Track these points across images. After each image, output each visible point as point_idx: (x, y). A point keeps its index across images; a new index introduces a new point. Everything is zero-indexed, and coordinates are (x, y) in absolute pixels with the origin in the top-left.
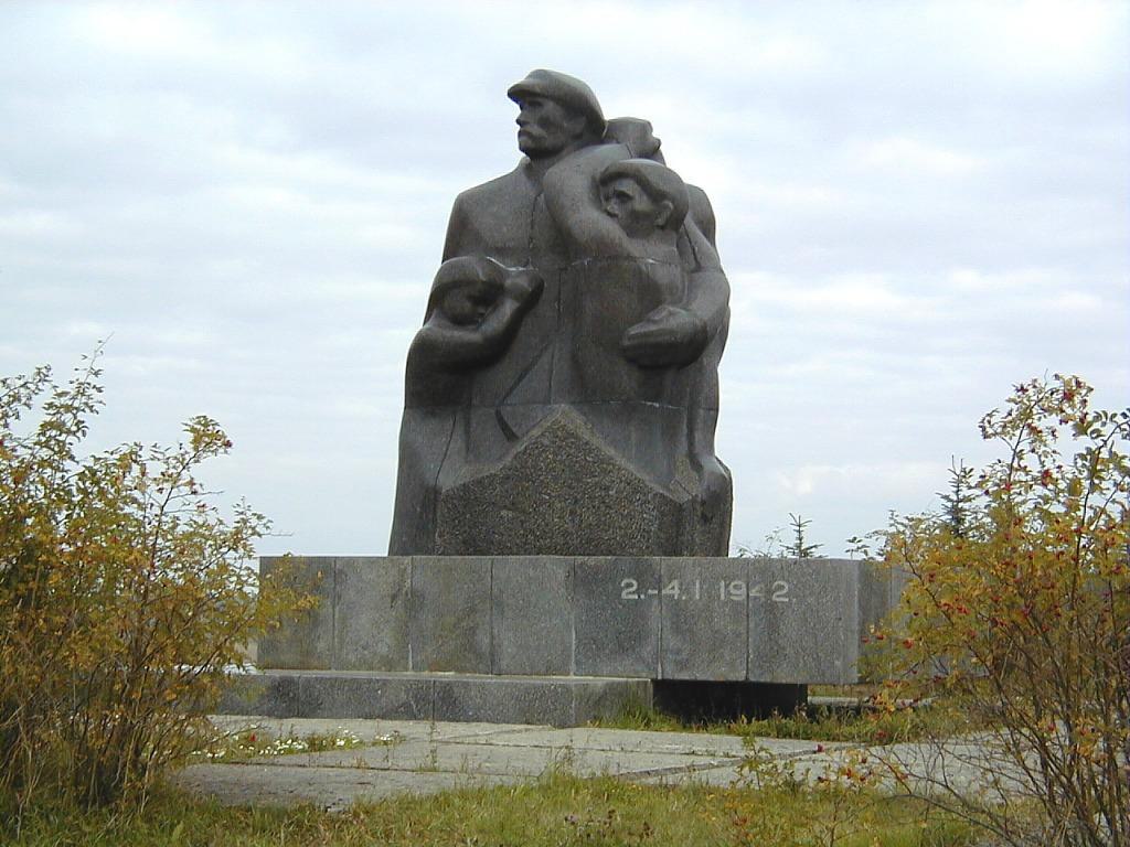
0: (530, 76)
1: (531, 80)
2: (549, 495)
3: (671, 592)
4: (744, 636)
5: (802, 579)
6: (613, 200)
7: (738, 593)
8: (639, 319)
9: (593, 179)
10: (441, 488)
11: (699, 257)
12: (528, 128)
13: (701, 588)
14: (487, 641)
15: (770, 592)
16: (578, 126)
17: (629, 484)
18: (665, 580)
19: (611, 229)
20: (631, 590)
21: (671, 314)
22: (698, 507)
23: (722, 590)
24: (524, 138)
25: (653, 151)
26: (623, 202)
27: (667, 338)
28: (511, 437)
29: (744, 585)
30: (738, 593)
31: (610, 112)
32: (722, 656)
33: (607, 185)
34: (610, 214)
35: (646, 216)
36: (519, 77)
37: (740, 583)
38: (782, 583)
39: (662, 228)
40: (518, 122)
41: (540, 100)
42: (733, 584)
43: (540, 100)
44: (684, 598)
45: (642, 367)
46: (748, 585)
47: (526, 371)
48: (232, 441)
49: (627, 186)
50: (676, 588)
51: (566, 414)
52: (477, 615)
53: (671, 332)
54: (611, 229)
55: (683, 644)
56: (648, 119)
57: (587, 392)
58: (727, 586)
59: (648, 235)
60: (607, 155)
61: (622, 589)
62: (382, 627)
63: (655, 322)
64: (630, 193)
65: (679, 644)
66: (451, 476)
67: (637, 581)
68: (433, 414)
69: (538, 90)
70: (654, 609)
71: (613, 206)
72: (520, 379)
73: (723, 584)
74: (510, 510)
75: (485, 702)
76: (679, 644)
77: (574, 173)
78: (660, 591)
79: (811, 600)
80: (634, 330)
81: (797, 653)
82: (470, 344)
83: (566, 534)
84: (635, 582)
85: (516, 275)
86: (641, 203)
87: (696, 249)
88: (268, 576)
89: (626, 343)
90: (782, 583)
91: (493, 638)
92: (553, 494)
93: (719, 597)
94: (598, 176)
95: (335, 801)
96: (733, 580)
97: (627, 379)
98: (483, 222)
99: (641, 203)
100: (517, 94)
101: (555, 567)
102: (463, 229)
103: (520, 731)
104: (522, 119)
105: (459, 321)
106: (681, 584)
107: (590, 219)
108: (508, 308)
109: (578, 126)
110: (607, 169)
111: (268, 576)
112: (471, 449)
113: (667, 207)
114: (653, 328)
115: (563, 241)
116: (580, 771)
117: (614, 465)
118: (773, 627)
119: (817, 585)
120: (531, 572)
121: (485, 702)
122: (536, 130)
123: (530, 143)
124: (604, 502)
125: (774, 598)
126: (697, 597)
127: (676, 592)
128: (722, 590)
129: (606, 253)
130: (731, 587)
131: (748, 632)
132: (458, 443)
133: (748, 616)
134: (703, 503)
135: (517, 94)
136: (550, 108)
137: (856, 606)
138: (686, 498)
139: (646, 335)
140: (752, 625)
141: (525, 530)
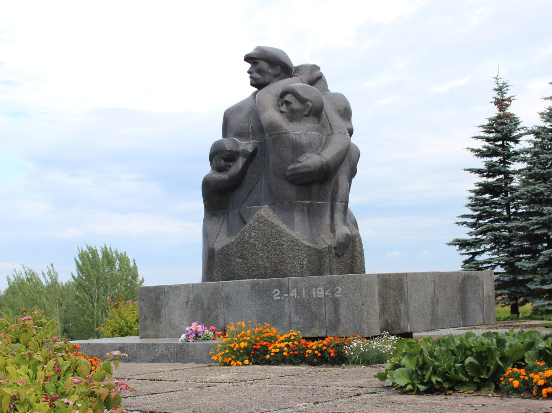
0: (254, 50)
1: (255, 51)
2: (256, 250)
3: (293, 295)
4: (324, 315)
5: (347, 285)
6: (284, 105)
7: (321, 293)
8: (293, 162)
9: (277, 96)
10: (215, 250)
11: (333, 127)
12: (253, 75)
13: (305, 292)
14: (223, 322)
15: (333, 292)
16: (278, 70)
17: (292, 242)
18: (290, 288)
20: (278, 294)
21: (308, 158)
22: (333, 250)
23: (314, 292)
26: (288, 105)
27: (306, 169)
28: (245, 223)
29: (323, 290)
30: (321, 293)
31: (296, 61)
32: (315, 325)
34: (282, 112)
35: (298, 111)
36: (250, 50)
37: (321, 288)
38: (338, 288)
39: (307, 116)
40: (249, 72)
41: (257, 61)
42: (318, 289)
43: (257, 61)
44: (299, 297)
45: (297, 185)
46: (324, 290)
47: (251, 191)
49: (288, 98)
50: (295, 292)
52: (219, 310)
53: (308, 167)
55: (300, 320)
56: (320, 67)
58: (316, 290)
59: (300, 120)
61: (274, 294)
62: (183, 317)
63: (300, 162)
64: (290, 101)
65: (298, 320)
67: (279, 290)
68: (215, 215)
69: (255, 56)
70: (287, 304)
71: (284, 108)
72: (248, 195)
73: (314, 290)
74: (241, 258)
75: (195, 354)
76: (298, 320)
78: (289, 295)
79: (351, 295)
80: (290, 167)
81: (346, 322)
82: (223, 181)
83: (265, 268)
84: (279, 291)
86: (296, 105)
87: (332, 124)
89: (288, 174)
90: (338, 288)
91: (225, 320)
92: (258, 249)
93: (313, 296)
94: (279, 94)
95: (317, 371)
96: (318, 287)
97: (290, 191)
98: (234, 122)
99: (296, 105)
100: (248, 59)
101: (246, 283)
104: (250, 71)
106: (297, 291)
108: (241, 162)
109: (278, 70)
110: (284, 88)
112: (230, 232)
113: (308, 105)
114: (299, 165)
116: (471, 342)
117: (285, 233)
118: (336, 310)
119: (353, 288)
120: (238, 288)
121: (195, 354)
122: (257, 75)
123: (254, 82)
124: (281, 252)
125: (336, 296)
126: (304, 297)
127: (295, 294)
128: (314, 292)
130: (317, 291)
131: (325, 312)
132: (224, 228)
133: (325, 305)
134: (335, 248)
135: (248, 59)
137: (377, 297)
138: (325, 246)
139: (295, 169)
140: (327, 309)
141: (247, 267)
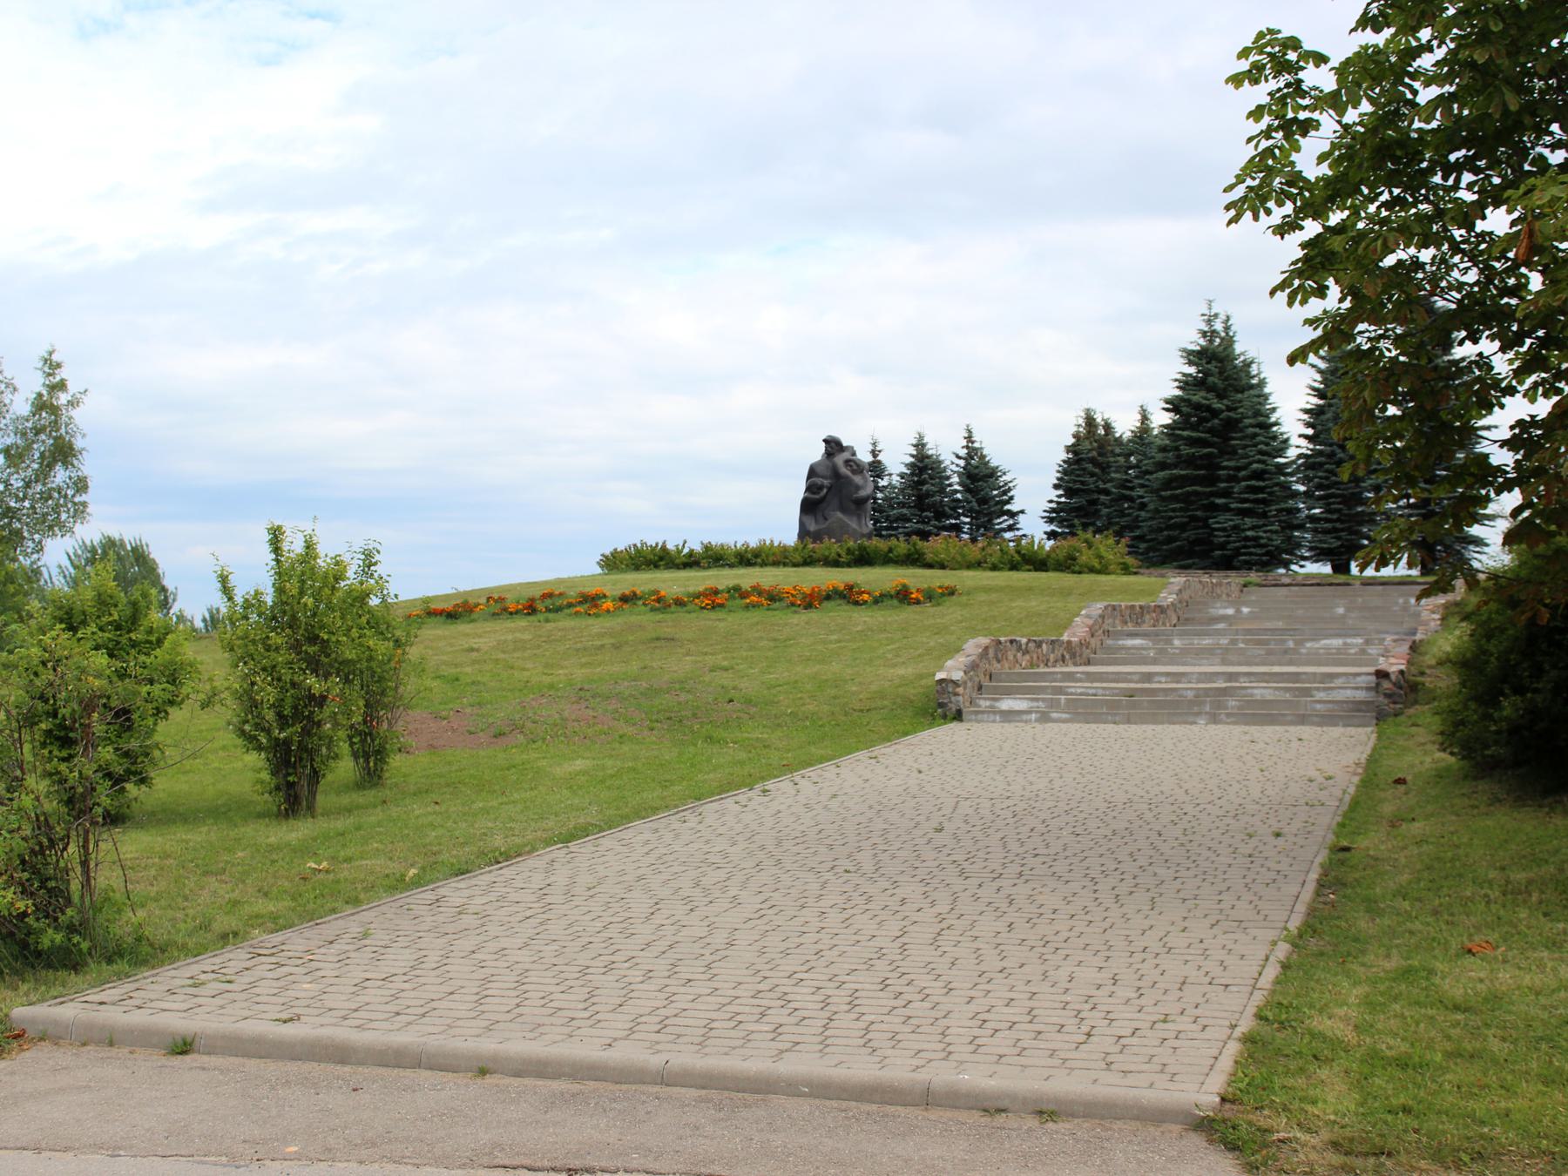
19: (849, 473)
24: (1400, 677)
25: (854, 454)
28: (826, 519)
31: (845, 444)
33: (847, 462)
36: (824, 437)
48: (1506, 408)
51: (839, 514)
54: (849, 473)
57: (844, 510)
60: (846, 455)
66: (812, 527)
77: (839, 460)
85: (826, 482)
86: (855, 467)
88: (1536, 282)
97: (853, 507)
99: (855, 467)
100: (824, 441)
102: (812, 472)
103: (811, 601)
105: (814, 493)
107: (844, 471)
108: (825, 491)
111: (1536, 282)
115: (836, 474)
129: (847, 477)
135: (824, 441)
136: (833, 444)
